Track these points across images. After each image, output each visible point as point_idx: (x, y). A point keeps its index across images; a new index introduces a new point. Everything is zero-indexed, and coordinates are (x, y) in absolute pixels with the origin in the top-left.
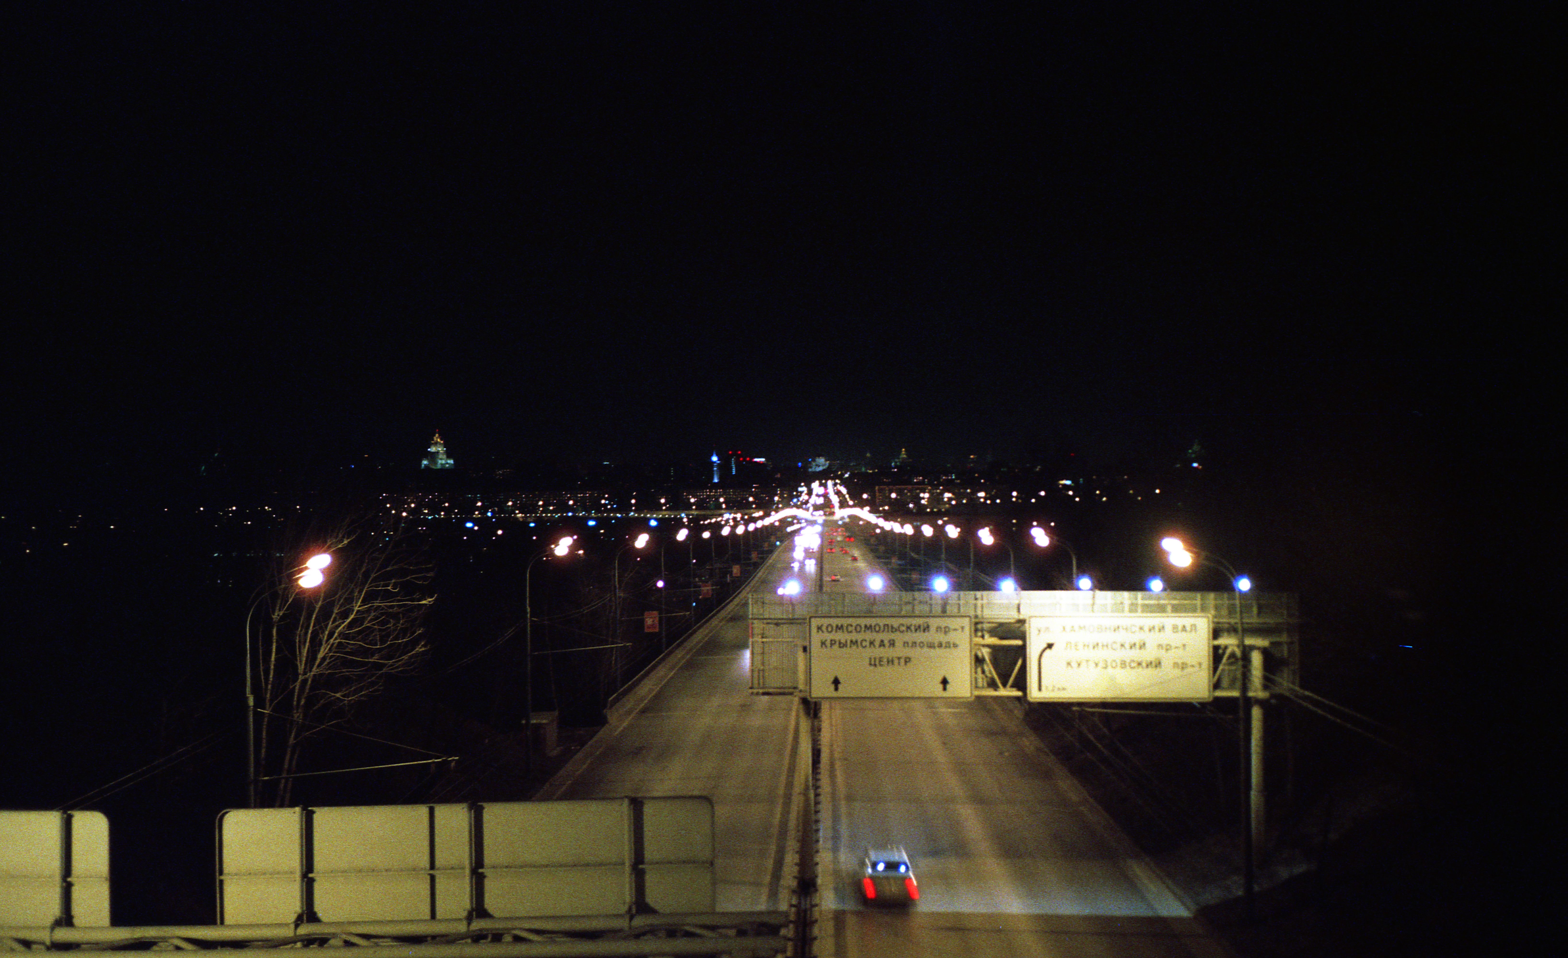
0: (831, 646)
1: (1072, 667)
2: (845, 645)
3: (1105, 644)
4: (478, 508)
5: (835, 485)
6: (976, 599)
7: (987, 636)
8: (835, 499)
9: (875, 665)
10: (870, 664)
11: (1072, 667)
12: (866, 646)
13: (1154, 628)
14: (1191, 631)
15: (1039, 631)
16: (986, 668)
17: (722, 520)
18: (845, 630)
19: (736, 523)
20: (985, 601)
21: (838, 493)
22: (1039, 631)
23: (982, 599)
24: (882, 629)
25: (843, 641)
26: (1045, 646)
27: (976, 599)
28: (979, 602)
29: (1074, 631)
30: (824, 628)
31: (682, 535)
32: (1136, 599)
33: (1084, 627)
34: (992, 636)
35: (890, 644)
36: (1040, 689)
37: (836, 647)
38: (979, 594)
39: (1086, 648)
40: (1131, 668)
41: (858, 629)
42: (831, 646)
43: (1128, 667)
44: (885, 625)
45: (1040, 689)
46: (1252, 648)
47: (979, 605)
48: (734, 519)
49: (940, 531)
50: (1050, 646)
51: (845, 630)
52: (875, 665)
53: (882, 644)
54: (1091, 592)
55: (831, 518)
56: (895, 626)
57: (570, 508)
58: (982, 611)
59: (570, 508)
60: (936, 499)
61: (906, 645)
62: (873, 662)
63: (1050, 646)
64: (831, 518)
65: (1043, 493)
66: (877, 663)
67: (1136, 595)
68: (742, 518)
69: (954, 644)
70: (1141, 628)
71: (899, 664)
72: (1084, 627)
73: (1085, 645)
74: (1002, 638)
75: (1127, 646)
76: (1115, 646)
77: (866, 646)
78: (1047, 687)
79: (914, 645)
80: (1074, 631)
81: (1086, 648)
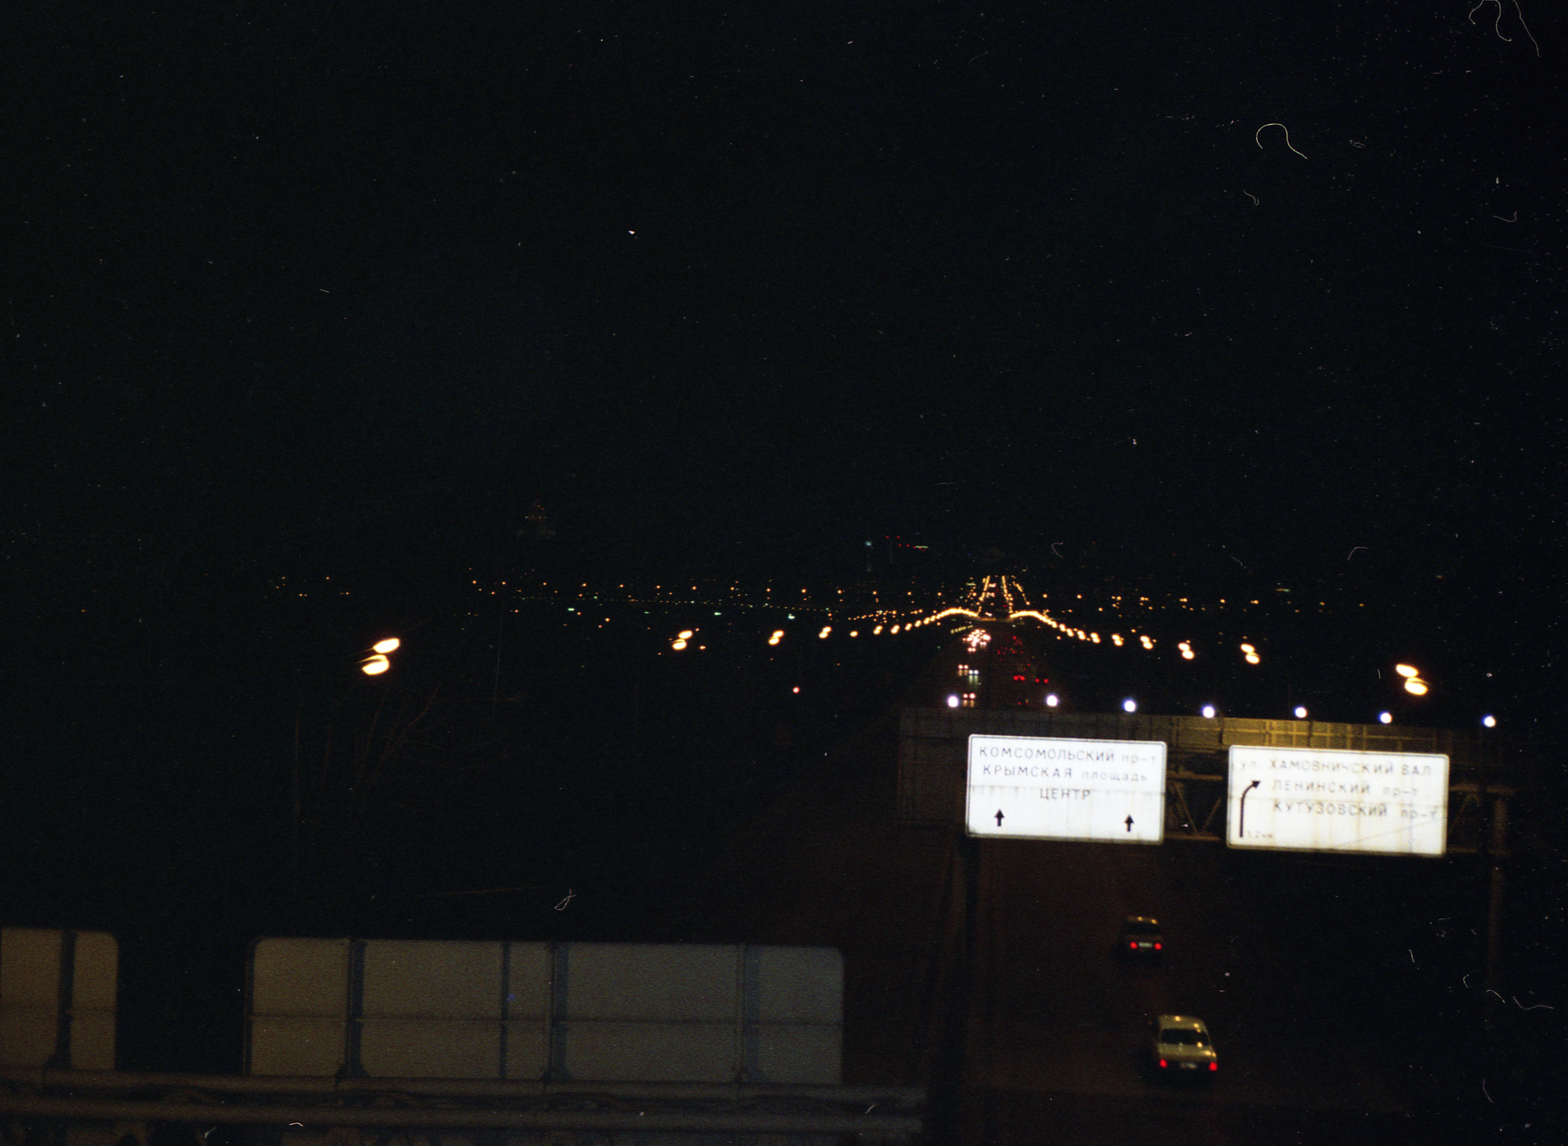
0: (995, 773)
1: (1280, 810)
2: (1012, 773)
3: (1299, 783)
4: (583, 590)
5: (1009, 581)
6: (1172, 724)
7: (1181, 769)
8: (1008, 597)
9: (1047, 798)
10: (1042, 797)
11: (1280, 810)
12: (1037, 775)
13: (1380, 767)
14: (1423, 774)
15: (1244, 765)
16: (1179, 806)
17: (874, 617)
18: (1047, 756)
19: (891, 623)
20: (1181, 728)
21: (1013, 590)
22: (1244, 765)
23: (1178, 725)
24: (1057, 755)
25: (1010, 768)
26: (1250, 783)
27: (1172, 724)
28: (1175, 729)
29: (1285, 767)
30: (988, 751)
31: (878, 630)
32: (1361, 733)
33: (1298, 763)
34: (1188, 768)
35: (1067, 774)
36: (1241, 835)
37: (1001, 773)
38: (1175, 718)
39: (1299, 788)
40: (1351, 814)
41: (995, 752)
42: (995, 773)
43: (1347, 814)
44: (1060, 751)
45: (1241, 835)
46: (1496, 797)
47: (1175, 732)
48: (889, 616)
49: (1132, 642)
50: (1255, 784)
51: (1047, 756)
52: (1047, 798)
53: (1057, 772)
54: (1308, 723)
55: (1002, 621)
56: (1074, 752)
57: (693, 595)
58: (1177, 739)
59: (693, 595)
60: (1130, 602)
61: (1085, 775)
62: (1044, 795)
63: (1255, 784)
64: (1002, 621)
65: (697, 630)
66: (1050, 796)
67: (1345, 726)
68: (898, 615)
69: (1143, 777)
70: (1089, 755)
71: (1076, 798)
72: (1298, 763)
73: (1297, 785)
74: (1197, 773)
75: (1348, 789)
76: (1333, 787)
77: (1037, 775)
78: (1249, 832)
79: (1095, 776)
80: (1285, 767)
81: (1321, 789)
